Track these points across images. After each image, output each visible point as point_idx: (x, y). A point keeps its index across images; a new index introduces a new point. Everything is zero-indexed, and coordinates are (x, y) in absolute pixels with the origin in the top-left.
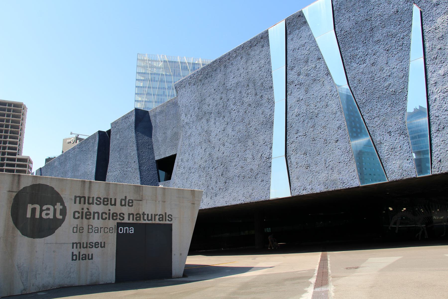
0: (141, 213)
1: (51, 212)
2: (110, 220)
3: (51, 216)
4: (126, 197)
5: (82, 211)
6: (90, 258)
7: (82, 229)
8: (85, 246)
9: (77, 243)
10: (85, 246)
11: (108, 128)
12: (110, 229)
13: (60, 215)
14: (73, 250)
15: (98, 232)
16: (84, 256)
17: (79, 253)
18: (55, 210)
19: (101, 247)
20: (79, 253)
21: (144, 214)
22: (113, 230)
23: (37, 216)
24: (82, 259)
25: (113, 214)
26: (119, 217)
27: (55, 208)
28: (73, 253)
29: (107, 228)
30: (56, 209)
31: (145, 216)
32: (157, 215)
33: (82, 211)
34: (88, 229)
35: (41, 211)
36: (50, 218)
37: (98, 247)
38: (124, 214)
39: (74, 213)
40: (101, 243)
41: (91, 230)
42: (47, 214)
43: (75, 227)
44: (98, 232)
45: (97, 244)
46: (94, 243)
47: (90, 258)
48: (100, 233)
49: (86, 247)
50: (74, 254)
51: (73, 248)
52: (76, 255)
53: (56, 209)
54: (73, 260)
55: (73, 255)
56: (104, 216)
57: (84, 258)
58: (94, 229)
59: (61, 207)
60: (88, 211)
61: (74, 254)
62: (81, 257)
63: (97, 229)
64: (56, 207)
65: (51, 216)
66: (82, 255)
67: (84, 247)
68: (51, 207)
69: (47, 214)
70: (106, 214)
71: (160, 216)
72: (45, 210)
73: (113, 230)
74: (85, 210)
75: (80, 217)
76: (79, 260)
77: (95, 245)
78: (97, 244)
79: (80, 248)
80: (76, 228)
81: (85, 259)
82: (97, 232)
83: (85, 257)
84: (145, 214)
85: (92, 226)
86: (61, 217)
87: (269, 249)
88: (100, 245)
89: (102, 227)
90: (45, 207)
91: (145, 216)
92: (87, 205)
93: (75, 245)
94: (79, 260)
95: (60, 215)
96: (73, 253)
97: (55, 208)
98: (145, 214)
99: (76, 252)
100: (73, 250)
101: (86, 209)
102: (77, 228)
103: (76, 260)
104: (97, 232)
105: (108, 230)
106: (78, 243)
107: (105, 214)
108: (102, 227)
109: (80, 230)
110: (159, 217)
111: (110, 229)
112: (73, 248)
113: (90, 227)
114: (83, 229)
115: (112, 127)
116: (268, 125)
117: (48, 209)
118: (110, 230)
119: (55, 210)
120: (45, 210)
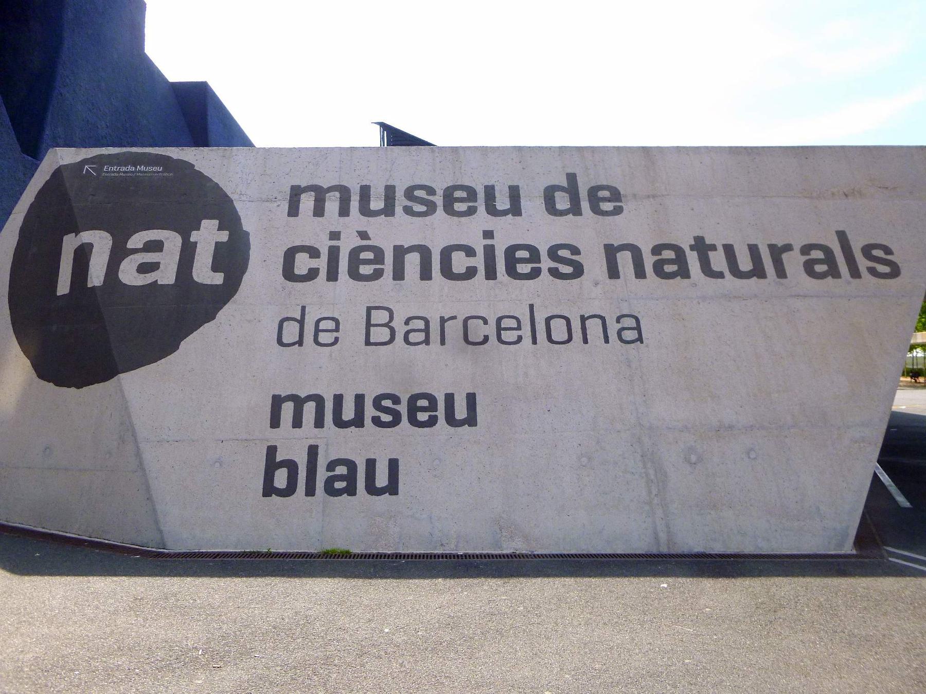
0: (685, 243)
2: (336, 279)
4: (572, 178)
5: (334, 243)
6: (382, 480)
7: (330, 325)
12: (321, 328)
13: (215, 268)
15: (427, 341)
16: (341, 470)
17: (313, 451)
19: (451, 420)
20: (313, 451)
21: (702, 247)
22: (519, 328)
23: (96, 276)
24: (331, 491)
25: (511, 251)
26: (546, 263)
27: (192, 239)
28: (272, 451)
29: (481, 322)
31: (711, 254)
32: (788, 248)
33: (334, 243)
34: (369, 325)
35: (118, 254)
38: (575, 251)
39: (290, 255)
40: (338, 400)
41: (386, 331)
43: (288, 319)
44: (427, 341)
47: (382, 480)
48: (443, 342)
49: (358, 421)
50: (278, 459)
52: (292, 466)
54: (269, 489)
56: (460, 262)
57: (340, 485)
58: (401, 330)
59: (224, 236)
60: (365, 243)
61: (278, 459)
62: (322, 475)
63: (321, 334)
64: (194, 236)
65: (167, 275)
66: (331, 466)
67: (340, 423)
68: (172, 241)
70: (314, 253)
71: (809, 254)
72: (135, 251)
73: (519, 328)
74: (347, 245)
75: (323, 273)
76: (310, 491)
79: (319, 423)
80: (297, 325)
81: (351, 490)
82: (293, 344)
83: (351, 479)
84: (713, 248)
85: (390, 311)
86: (218, 279)
89: (454, 318)
90: (137, 240)
91: (711, 254)
92: (356, 220)
93: (288, 409)
95: (215, 268)
96: (272, 451)
97: (192, 239)
98: (713, 248)
101: (895, 252)
102: (301, 322)
104: (293, 344)
105: (491, 330)
107: (464, 254)
108: (454, 318)
109: (321, 334)
110: (808, 257)
111: (321, 328)
113: (380, 317)
114: (337, 329)
117: (155, 246)
118: (499, 329)
119: (188, 253)
120: (135, 251)
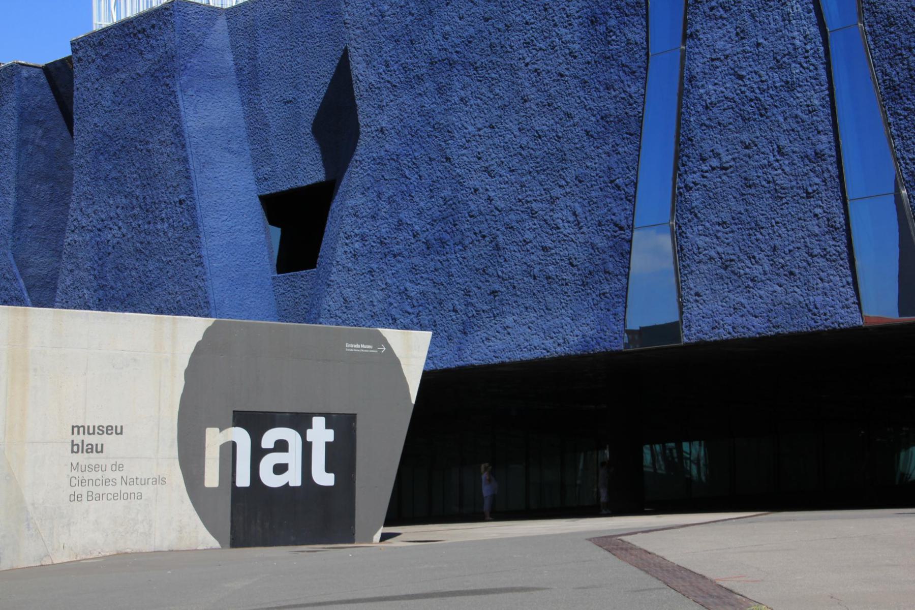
1: (293, 458)
3: (294, 478)
8: (91, 431)
9: (78, 427)
10: (91, 431)
11: (67, 52)
13: (328, 470)
14: (72, 437)
16: (90, 447)
17: (83, 441)
18: (307, 448)
20: (83, 441)
28: (73, 441)
30: (311, 443)
36: (291, 485)
37: (112, 433)
42: (280, 469)
45: (110, 428)
46: (105, 426)
47: (99, 449)
49: (94, 433)
51: (73, 433)
52: (78, 445)
53: (311, 443)
54: (73, 452)
55: (73, 445)
57: (89, 450)
62: (85, 448)
66: (87, 446)
69: (280, 469)
76: (82, 452)
77: (107, 430)
78: (110, 428)
81: (92, 452)
83: (92, 449)
87: (607, 452)
88: (114, 431)
90: (269, 439)
93: (76, 429)
94: (82, 452)
95: (328, 470)
96: (73, 441)
99: (78, 439)
100: (72, 437)
103: (78, 452)
106: (81, 426)
112: (73, 433)
115: (74, 51)
116: (208, 118)
117: (282, 446)
119: (307, 448)
